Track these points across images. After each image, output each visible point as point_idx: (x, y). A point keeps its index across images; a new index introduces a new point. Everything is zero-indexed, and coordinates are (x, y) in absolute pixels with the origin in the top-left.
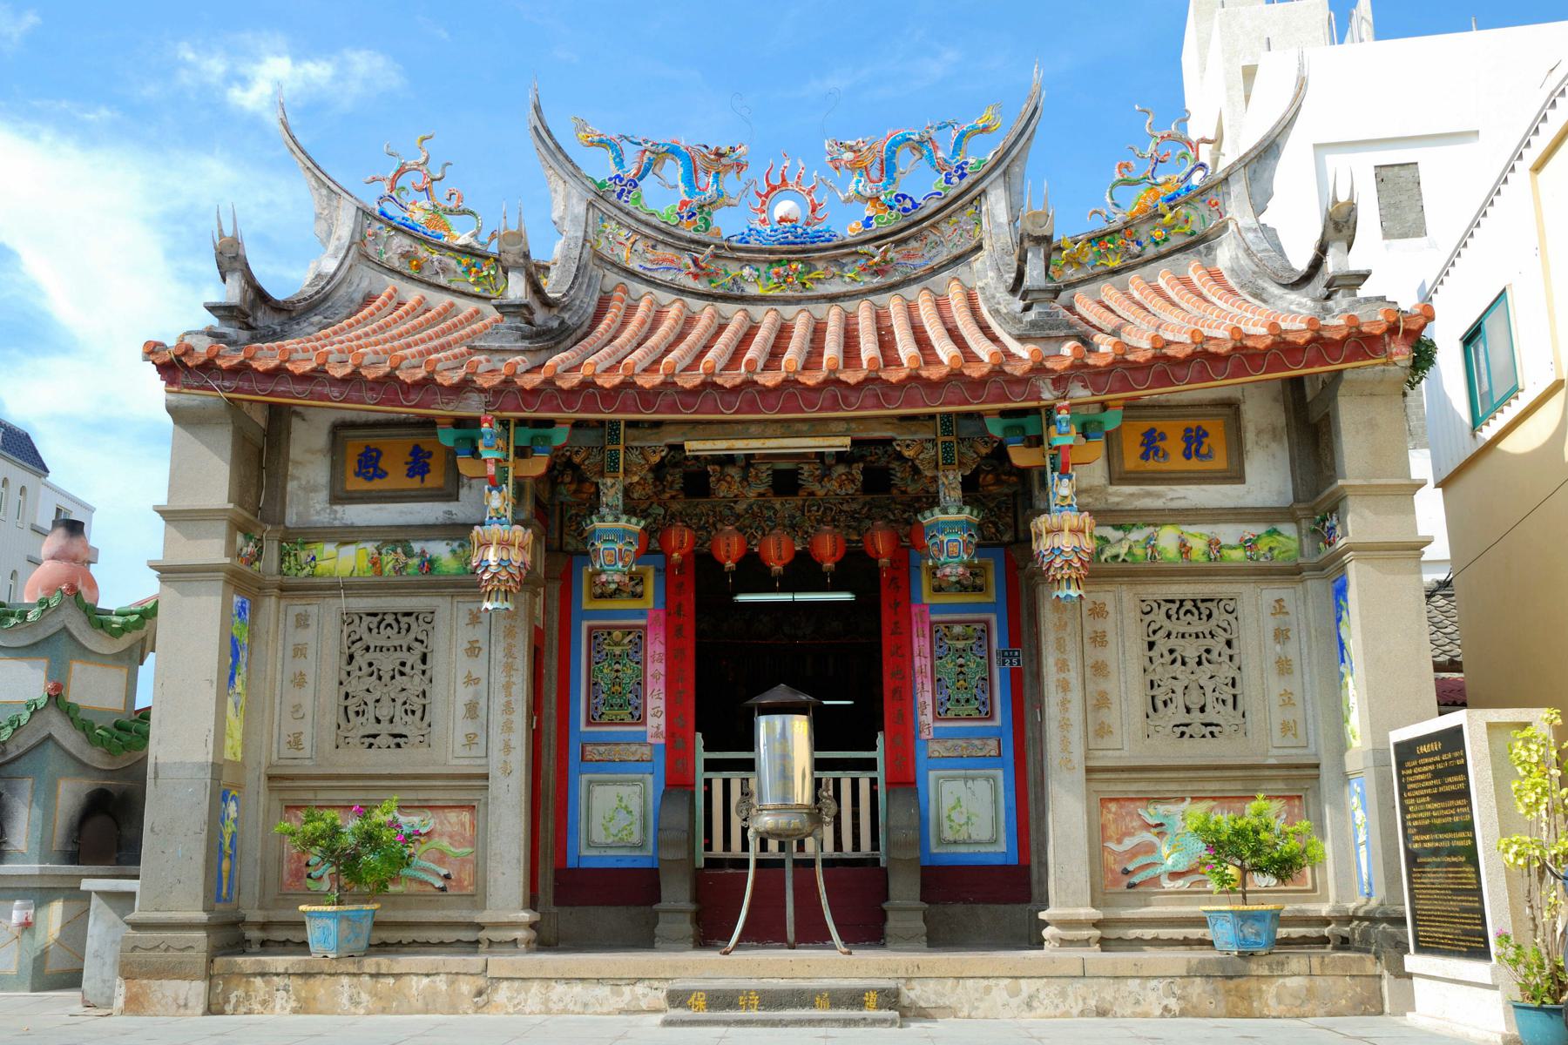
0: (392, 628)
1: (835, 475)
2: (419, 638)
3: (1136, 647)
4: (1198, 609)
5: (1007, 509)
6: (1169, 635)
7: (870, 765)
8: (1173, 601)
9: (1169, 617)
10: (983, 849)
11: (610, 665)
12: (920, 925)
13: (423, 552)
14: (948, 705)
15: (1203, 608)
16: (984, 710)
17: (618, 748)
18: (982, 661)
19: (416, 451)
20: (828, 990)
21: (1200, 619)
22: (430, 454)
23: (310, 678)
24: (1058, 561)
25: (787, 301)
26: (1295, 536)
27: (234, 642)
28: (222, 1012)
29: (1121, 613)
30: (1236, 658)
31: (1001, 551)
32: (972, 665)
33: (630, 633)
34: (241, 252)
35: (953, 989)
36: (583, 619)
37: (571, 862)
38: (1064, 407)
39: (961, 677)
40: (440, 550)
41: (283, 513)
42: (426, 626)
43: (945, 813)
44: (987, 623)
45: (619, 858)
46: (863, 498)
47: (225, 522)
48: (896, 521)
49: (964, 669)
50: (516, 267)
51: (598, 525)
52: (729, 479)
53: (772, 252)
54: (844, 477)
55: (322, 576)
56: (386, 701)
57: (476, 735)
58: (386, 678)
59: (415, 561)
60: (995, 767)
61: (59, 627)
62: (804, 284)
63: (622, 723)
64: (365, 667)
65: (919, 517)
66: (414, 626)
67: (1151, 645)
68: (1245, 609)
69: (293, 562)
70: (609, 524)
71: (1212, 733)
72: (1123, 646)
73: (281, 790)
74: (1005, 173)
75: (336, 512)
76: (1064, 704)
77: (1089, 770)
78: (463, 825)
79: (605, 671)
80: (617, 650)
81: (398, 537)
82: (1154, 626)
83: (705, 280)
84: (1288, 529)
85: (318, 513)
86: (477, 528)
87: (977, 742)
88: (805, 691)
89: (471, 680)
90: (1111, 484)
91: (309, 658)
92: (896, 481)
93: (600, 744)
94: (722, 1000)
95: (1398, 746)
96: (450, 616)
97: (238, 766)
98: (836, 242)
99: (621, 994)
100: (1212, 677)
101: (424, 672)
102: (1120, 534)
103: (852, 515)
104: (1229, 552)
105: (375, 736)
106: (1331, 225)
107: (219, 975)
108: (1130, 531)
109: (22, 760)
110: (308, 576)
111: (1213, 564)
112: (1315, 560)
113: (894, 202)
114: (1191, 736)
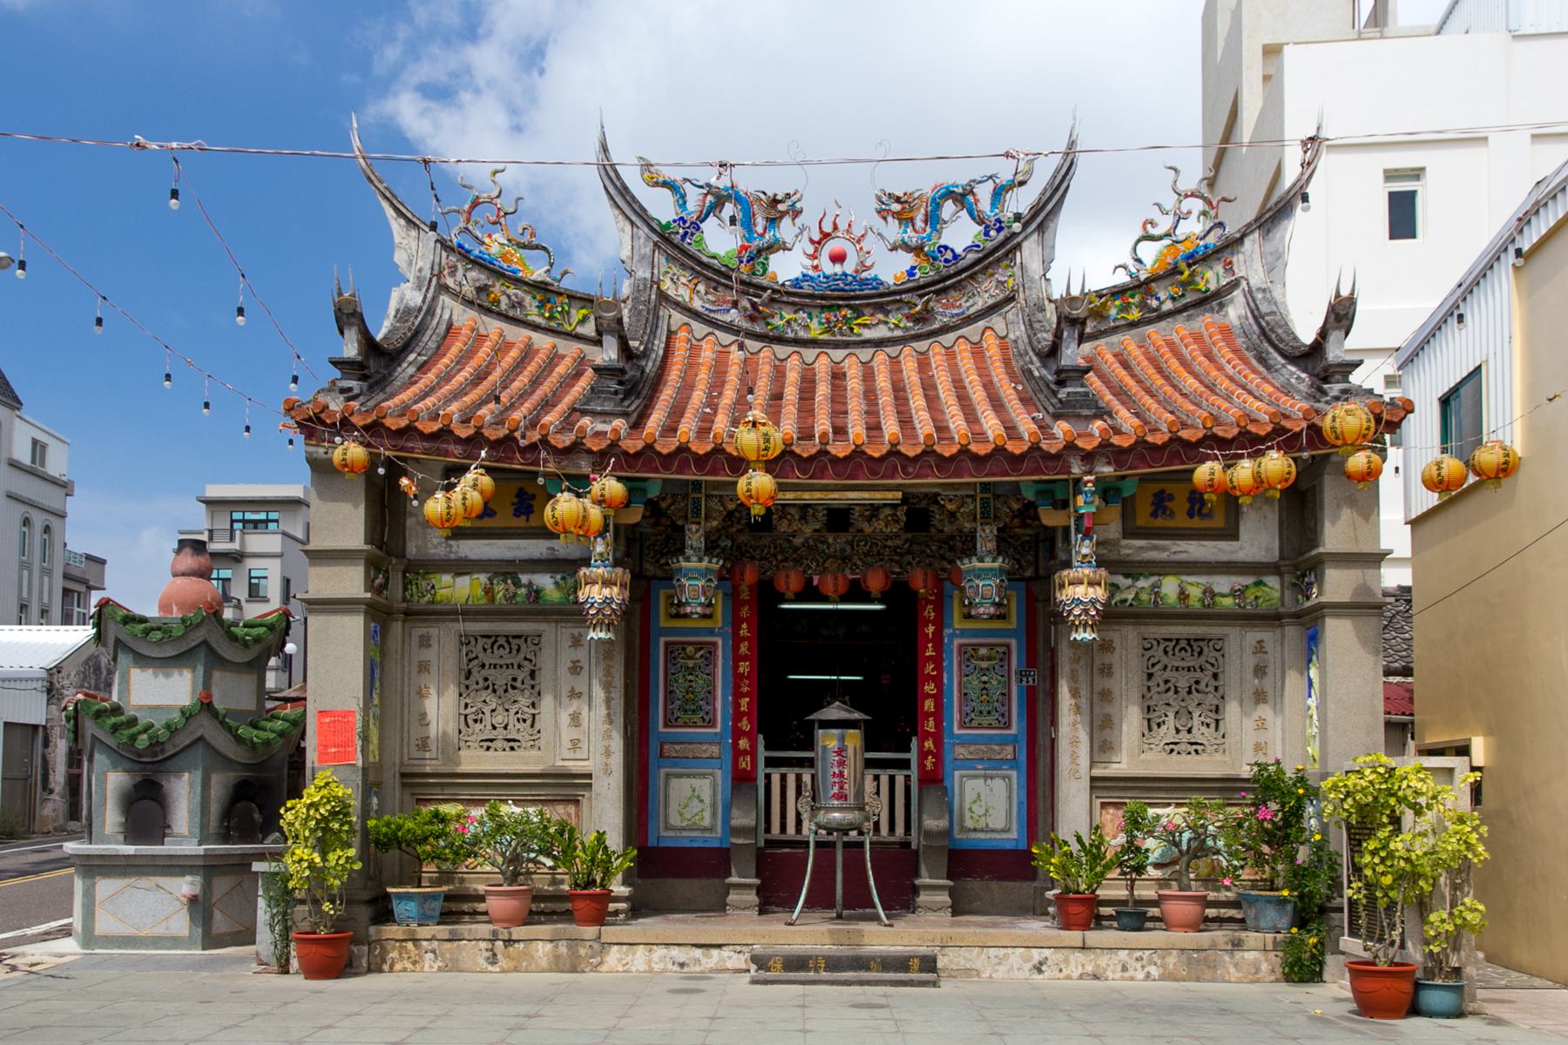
1: (882, 516)
4: (1191, 646)
5: (1030, 548)
6: (1165, 668)
7: (905, 764)
8: (1170, 640)
10: (997, 836)
12: (945, 898)
14: (973, 715)
15: (1193, 645)
17: (691, 747)
18: (1002, 679)
19: (521, 494)
22: (534, 497)
25: (837, 345)
26: (1278, 586)
27: (372, 661)
28: (381, 971)
30: (1221, 689)
31: (1022, 585)
32: (994, 683)
33: (701, 649)
34: (359, 310)
35: (979, 955)
37: (652, 842)
38: (1089, 481)
40: (546, 582)
41: (404, 547)
42: (533, 648)
43: (967, 806)
44: (1008, 646)
45: (693, 839)
46: (905, 536)
48: (933, 556)
49: (987, 686)
50: (611, 332)
51: (684, 564)
53: (823, 297)
55: (441, 602)
58: (500, 691)
59: (523, 591)
60: (1011, 768)
61: (200, 640)
63: (695, 725)
65: (958, 563)
66: (523, 647)
67: (1150, 676)
68: (1231, 647)
70: (694, 564)
71: (1196, 751)
75: (451, 546)
78: (569, 815)
80: (691, 663)
81: (506, 570)
82: (1153, 661)
83: (762, 323)
84: (1273, 581)
85: (435, 547)
87: (996, 748)
88: (859, 709)
90: (1124, 538)
92: (935, 522)
93: (676, 743)
96: (554, 636)
97: (379, 766)
98: (882, 289)
99: (711, 957)
101: (533, 687)
102: (1129, 581)
103: (895, 549)
105: (491, 740)
108: (1138, 579)
110: (429, 602)
111: (1207, 610)
112: (1293, 610)
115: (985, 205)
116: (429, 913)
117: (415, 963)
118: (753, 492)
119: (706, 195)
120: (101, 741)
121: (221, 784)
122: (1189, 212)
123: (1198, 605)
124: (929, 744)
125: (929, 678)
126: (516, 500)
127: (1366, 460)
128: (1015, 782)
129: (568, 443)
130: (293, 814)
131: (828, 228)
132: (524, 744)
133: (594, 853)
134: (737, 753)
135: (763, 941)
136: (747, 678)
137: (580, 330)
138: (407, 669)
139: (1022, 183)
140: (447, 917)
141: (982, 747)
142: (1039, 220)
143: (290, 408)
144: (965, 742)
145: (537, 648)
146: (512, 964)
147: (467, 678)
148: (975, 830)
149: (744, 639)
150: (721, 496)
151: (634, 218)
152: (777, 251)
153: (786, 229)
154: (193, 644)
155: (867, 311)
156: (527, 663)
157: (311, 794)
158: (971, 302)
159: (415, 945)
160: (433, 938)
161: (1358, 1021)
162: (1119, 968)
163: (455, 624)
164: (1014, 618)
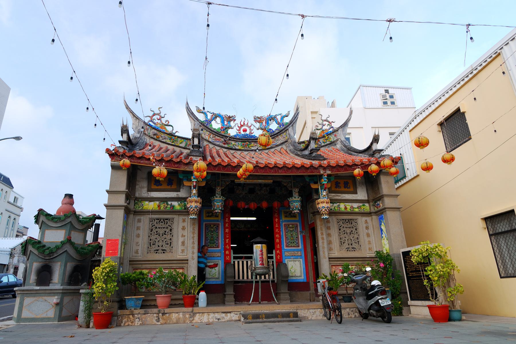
0: (163, 223)
1: (263, 190)
2: (170, 225)
3: (337, 230)
4: (349, 221)
7: (272, 258)
8: (344, 220)
9: (343, 223)
11: (210, 233)
13: (171, 204)
16: (297, 245)
17: (212, 254)
18: (296, 233)
20: (281, 313)
21: (350, 224)
22: (173, 180)
23: (141, 235)
24: (323, 209)
25: (245, 150)
29: (333, 222)
32: (294, 234)
33: (215, 225)
35: (307, 312)
36: (204, 222)
38: (326, 175)
39: (292, 237)
40: (176, 204)
42: (171, 222)
44: (297, 224)
47: (125, 194)
49: (292, 235)
50: (196, 137)
51: (215, 198)
52: (239, 189)
54: (265, 190)
56: (161, 241)
57: (184, 250)
58: (161, 235)
59: (169, 206)
61: (69, 221)
62: (249, 147)
64: (155, 233)
66: (168, 222)
67: (340, 229)
69: (137, 206)
71: (354, 250)
72: (334, 230)
73: (133, 264)
74: (292, 125)
75: (149, 193)
76: (323, 242)
77: (329, 258)
79: (209, 235)
80: (212, 230)
82: (340, 225)
84: (367, 205)
86: (189, 198)
87: (296, 252)
89: (183, 236)
90: (329, 193)
91: (141, 230)
94: (256, 317)
95: (403, 253)
99: (228, 316)
100: (353, 237)
101: (171, 234)
104: (355, 209)
105: (158, 250)
106: (374, 140)
107: (120, 315)
108: (334, 204)
109: (57, 257)
113: (269, 130)
114: (350, 251)
115: (279, 120)
116: (138, 305)
117: (132, 322)
118: (248, 168)
119: (213, 115)
120: (33, 252)
121: (70, 266)
122: (325, 124)
123: (350, 210)
124: (278, 252)
125: (277, 233)
126: (168, 181)
127: (396, 169)
128: (302, 262)
129: (187, 162)
130: (97, 272)
131: (242, 124)
132: (167, 251)
133: (191, 283)
134: (225, 255)
135: (244, 310)
136: (228, 234)
137: (181, 145)
138: (133, 229)
139: (287, 116)
140: (143, 307)
141: (292, 252)
142: (292, 124)
143: (108, 151)
144: (288, 251)
145: (172, 222)
146: (164, 322)
147: (151, 232)
148: (292, 276)
149: (227, 223)
150: (225, 181)
151: (195, 120)
152: (230, 128)
153: (232, 124)
154: (67, 223)
155: (253, 143)
156: (169, 227)
157: (103, 265)
158: (277, 142)
159: (133, 316)
160: (139, 313)
161: (435, 323)
162: (347, 314)
163: (148, 215)
164: (298, 217)
